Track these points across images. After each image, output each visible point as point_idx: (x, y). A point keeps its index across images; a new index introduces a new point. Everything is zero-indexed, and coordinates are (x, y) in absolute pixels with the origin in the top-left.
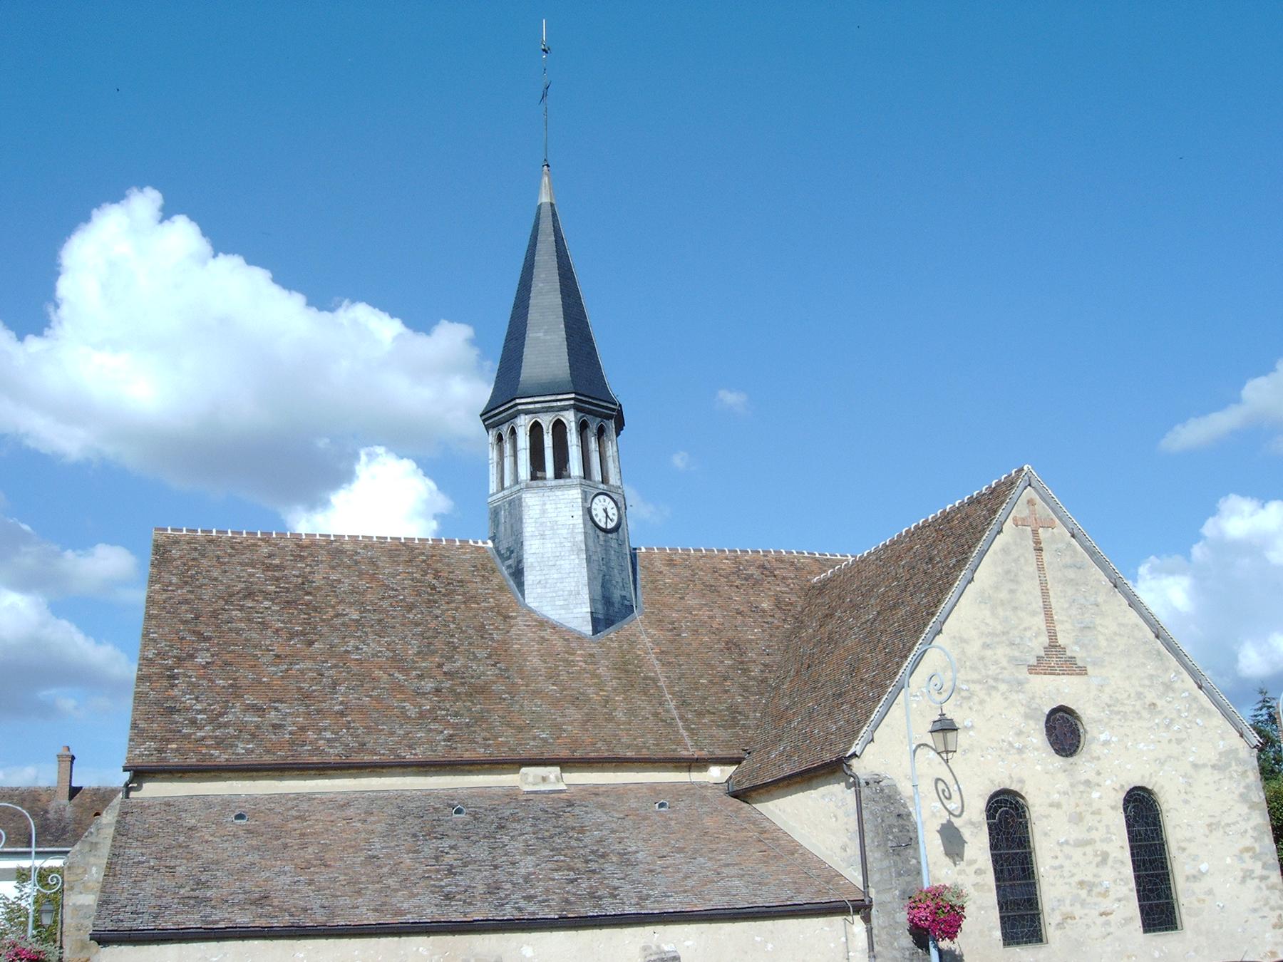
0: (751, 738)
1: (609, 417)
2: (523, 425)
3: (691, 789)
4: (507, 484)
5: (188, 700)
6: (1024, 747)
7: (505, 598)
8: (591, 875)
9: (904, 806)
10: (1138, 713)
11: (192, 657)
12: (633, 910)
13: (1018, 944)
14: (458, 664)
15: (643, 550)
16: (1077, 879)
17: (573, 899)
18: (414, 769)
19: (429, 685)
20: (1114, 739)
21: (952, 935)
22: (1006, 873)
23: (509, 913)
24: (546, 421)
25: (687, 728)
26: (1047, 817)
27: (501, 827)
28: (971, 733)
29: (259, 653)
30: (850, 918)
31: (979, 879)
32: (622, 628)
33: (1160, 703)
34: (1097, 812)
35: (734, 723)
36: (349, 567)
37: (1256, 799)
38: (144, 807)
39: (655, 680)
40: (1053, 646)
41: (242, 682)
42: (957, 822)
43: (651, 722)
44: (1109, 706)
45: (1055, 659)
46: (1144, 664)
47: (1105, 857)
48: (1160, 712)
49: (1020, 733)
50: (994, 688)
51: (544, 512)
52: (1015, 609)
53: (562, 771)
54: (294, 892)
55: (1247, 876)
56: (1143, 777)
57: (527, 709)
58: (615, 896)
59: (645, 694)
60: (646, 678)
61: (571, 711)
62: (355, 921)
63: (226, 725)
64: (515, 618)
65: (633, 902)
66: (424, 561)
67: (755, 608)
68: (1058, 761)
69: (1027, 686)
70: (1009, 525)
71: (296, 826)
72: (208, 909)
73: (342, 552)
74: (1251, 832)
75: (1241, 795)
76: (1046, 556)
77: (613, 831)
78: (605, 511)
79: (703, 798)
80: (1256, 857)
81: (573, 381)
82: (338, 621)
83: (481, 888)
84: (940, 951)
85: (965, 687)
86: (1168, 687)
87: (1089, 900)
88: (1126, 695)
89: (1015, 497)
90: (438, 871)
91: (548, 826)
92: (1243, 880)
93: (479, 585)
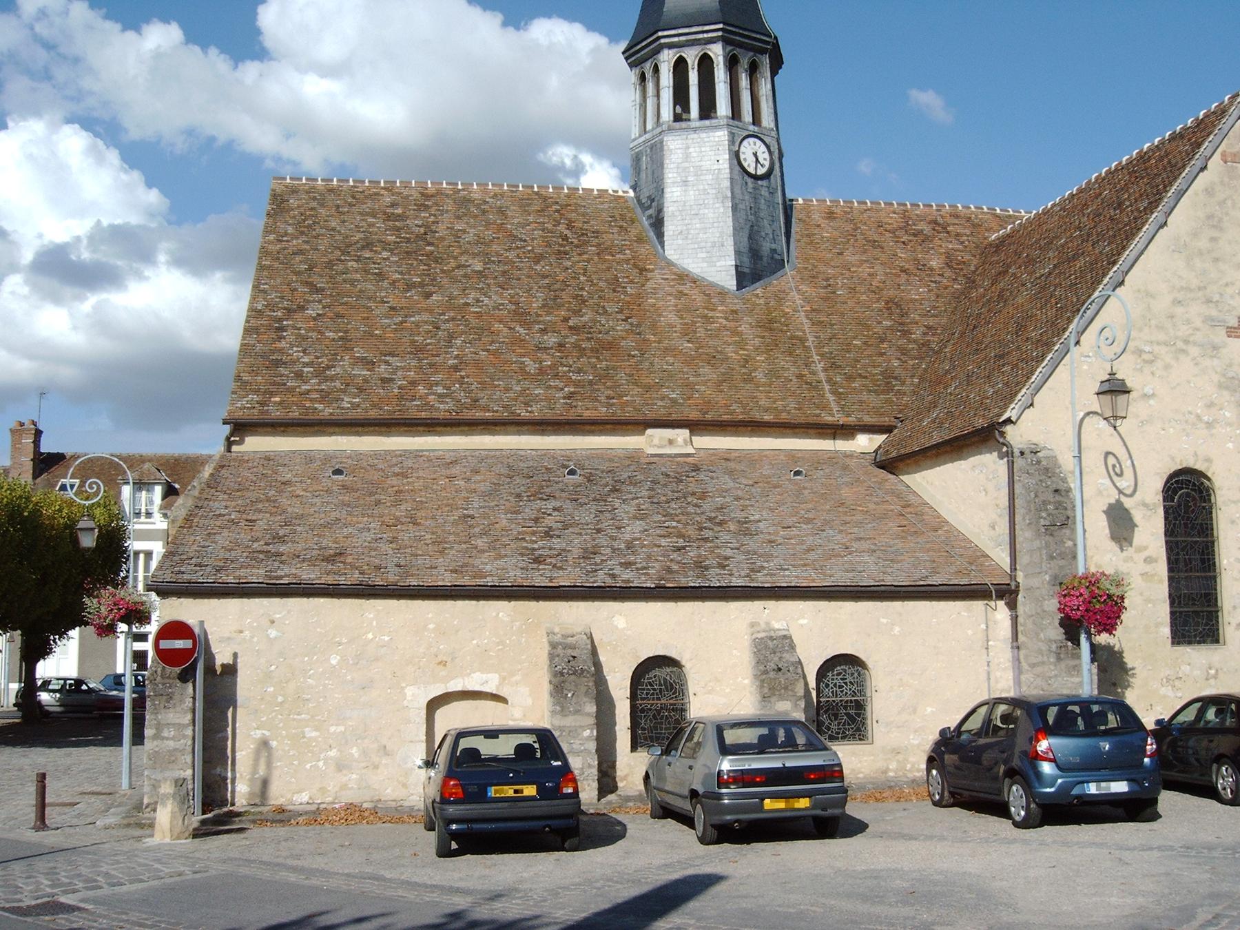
0: (906, 406)
1: (763, 52)
2: (667, 59)
3: (833, 459)
4: (649, 127)
5: (296, 352)
7: (643, 250)
8: (701, 543)
9: (1064, 480)
11: (302, 308)
12: (741, 582)
13: (1190, 643)
14: (585, 318)
15: (801, 201)
17: (675, 567)
21: (1109, 628)
22: (1181, 565)
23: (601, 579)
24: (692, 56)
25: (834, 392)
28: (1152, 402)
29: (372, 305)
30: (992, 603)
31: (1148, 568)
35: (889, 388)
36: (476, 216)
38: (242, 460)
39: (803, 340)
41: (351, 335)
42: (1128, 503)
43: (794, 385)
50: (1183, 351)
51: (687, 157)
52: (1216, 260)
54: (371, 549)
57: (657, 367)
58: (723, 567)
59: (790, 354)
60: (793, 337)
61: (706, 370)
62: (429, 581)
63: (332, 379)
64: (652, 271)
65: (743, 573)
66: (557, 211)
67: (922, 267)
69: (1224, 351)
70: (1215, 162)
71: (395, 483)
72: (276, 564)
73: (470, 201)
77: (738, 499)
78: (755, 155)
79: (845, 468)
81: (721, 10)
83: (576, 552)
85: (1147, 349)
89: (1226, 127)
90: (534, 533)
91: (667, 490)
93: (616, 236)
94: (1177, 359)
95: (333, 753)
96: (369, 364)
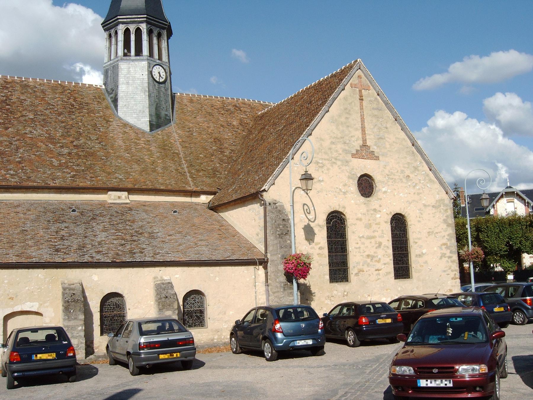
1: (164, 28)
2: (121, 29)
3: (191, 206)
6: (347, 191)
7: (108, 112)
8: (132, 242)
9: (287, 215)
10: (401, 179)
12: (150, 259)
13: (337, 282)
14: (81, 142)
15: (179, 94)
16: (366, 253)
17: (120, 253)
18: (55, 190)
19: (65, 151)
20: (389, 191)
21: (304, 277)
22: (334, 250)
23: (86, 259)
24: (132, 28)
26: (355, 224)
27: (93, 219)
28: (322, 183)
30: (257, 267)
31: (320, 252)
32: (164, 129)
33: (411, 176)
34: (378, 224)
35: (214, 175)
36: (31, 93)
37: (450, 222)
39: (178, 154)
40: (364, 145)
43: (174, 174)
44: (388, 175)
45: (365, 152)
46: (406, 157)
48: (411, 180)
49: (345, 185)
53: (129, 194)
55: (443, 256)
56: (401, 209)
57: (113, 164)
58: (142, 253)
59: (173, 160)
61: (135, 166)
65: (150, 255)
66: (69, 93)
67: (229, 124)
68: (362, 199)
69: (350, 163)
70: (348, 87)
73: (28, 86)
74: (446, 237)
75: (444, 220)
76: (365, 103)
77: (148, 223)
78: (159, 73)
79: (196, 209)
80: (447, 248)
81: (146, 9)
82: (22, 119)
83: (75, 247)
84: (299, 285)
85: (320, 162)
86: (416, 168)
87: (371, 263)
88: (396, 171)
89: (352, 73)
90: (56, 238)
92: (441, 258)
93: (96, 105)
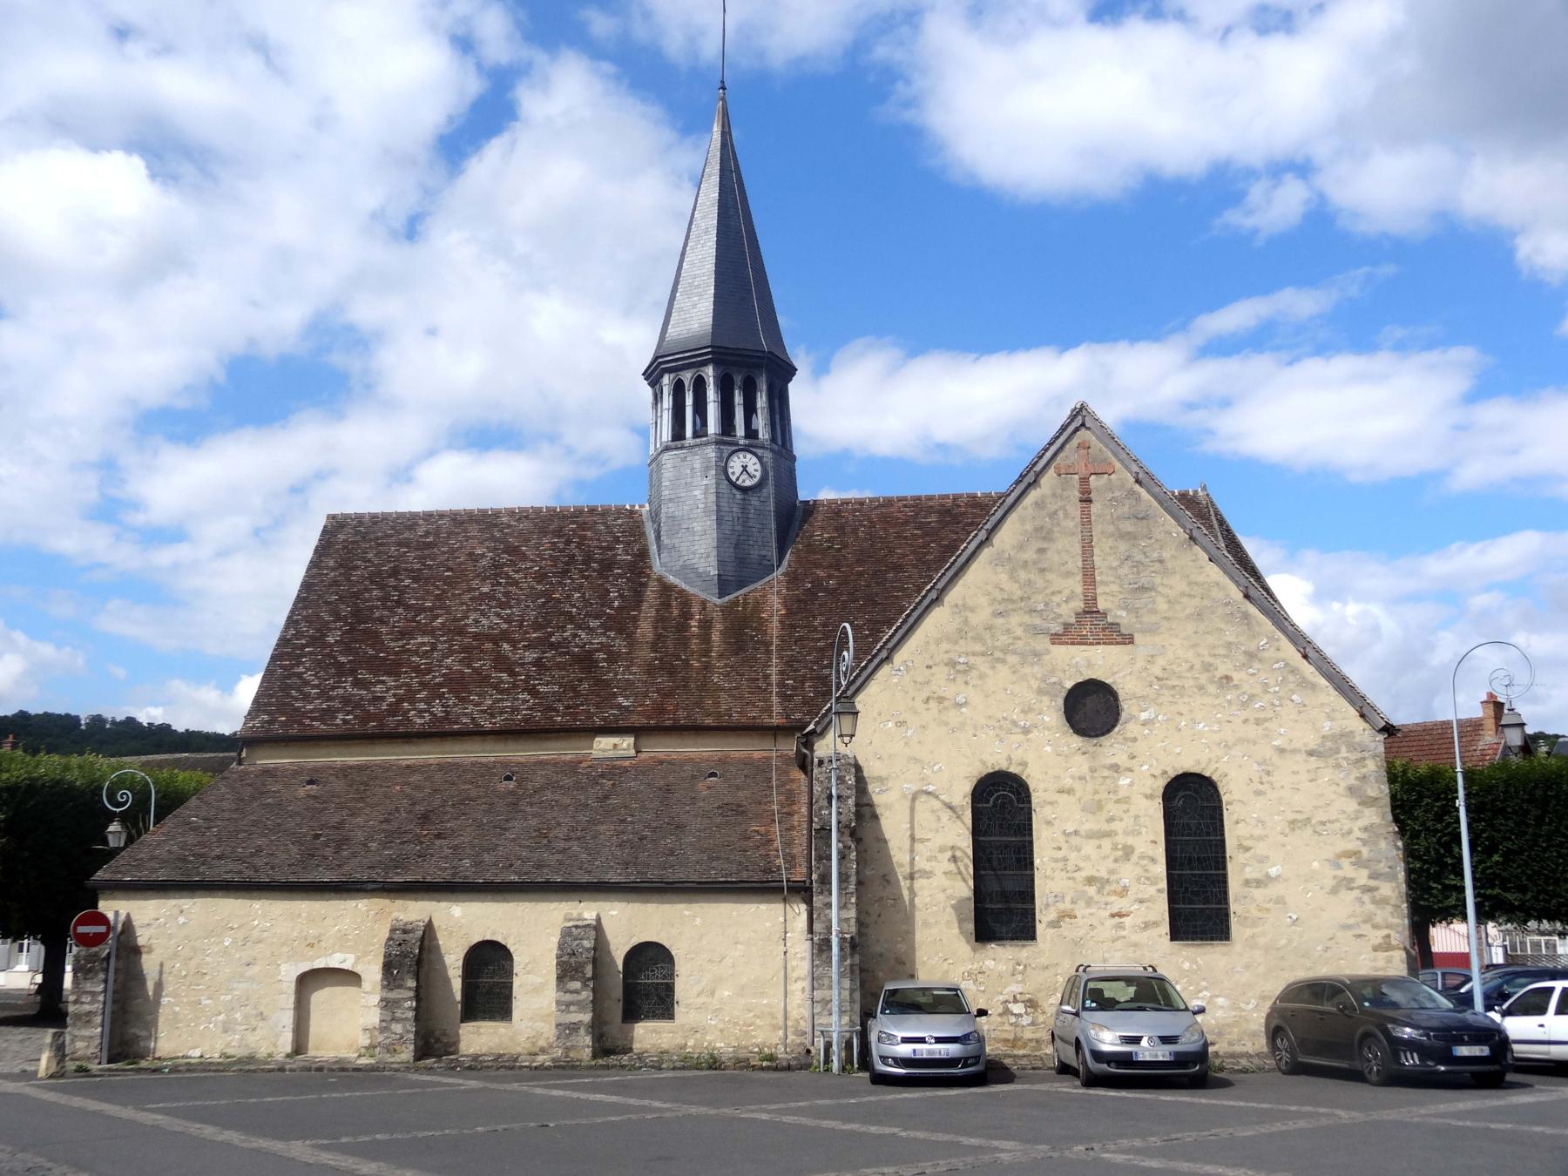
2: (666, 379)
16: (1084, 874)
40: (1090, 611)
47: (1128, 851)
52: (1042, 570)
68: (1077, 741)
69: (1046, 658)
76: (1095, 508)
94: (993, 667)
95: (221, 1018)
96: (358, 683)
